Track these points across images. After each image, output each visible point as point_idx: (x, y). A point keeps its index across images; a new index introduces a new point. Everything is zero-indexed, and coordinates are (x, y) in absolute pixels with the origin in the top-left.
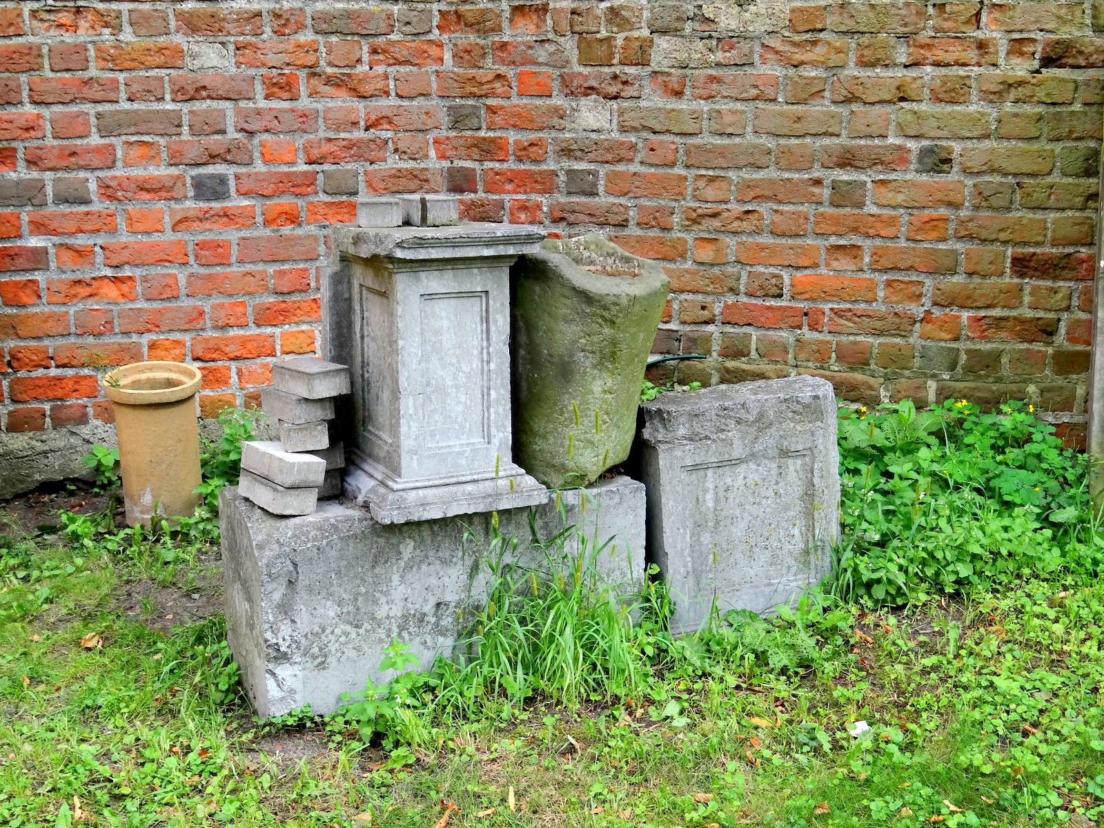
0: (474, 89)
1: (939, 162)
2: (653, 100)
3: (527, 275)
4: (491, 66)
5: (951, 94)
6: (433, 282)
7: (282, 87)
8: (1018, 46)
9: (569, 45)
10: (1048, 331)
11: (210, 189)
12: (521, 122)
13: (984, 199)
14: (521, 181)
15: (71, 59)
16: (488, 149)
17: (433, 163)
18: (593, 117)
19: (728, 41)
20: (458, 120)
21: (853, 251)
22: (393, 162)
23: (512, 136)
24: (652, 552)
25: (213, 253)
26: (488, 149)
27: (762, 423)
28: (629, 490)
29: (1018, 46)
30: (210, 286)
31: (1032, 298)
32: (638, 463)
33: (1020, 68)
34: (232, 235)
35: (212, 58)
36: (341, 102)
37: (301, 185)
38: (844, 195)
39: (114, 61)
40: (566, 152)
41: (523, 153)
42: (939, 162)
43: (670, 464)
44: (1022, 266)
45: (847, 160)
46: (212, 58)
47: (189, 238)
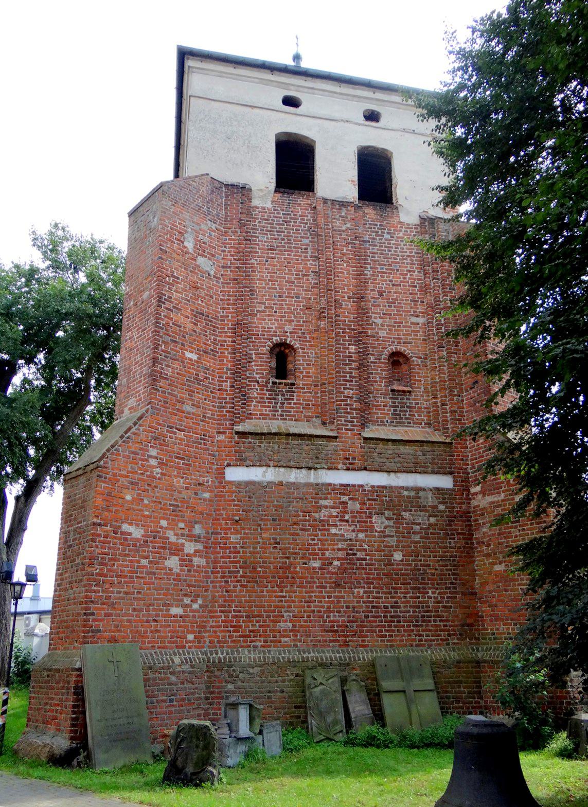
0: (210, 682)
1: (282, 691)
2: (240, 683)
3: (251, 706)
4: (213, 679)
5: (284, 681)
6: (243, 706)
7: (182, 683)
8: (292, 674)
9: (226, 675)
10: (299, 717)
11: (171, 701)
12: (218, 687)
13: (289, 697)
14: (218, 698)
15: (154, 679)
16: (212, 693)
17: (203, 695)
18: (230, 687)
19: (250, 674)
20: (207, 687)
21: (271, 706)
22: (197, 695)
23: (216, 690)
24: (263, 745)
25: (170, 712)
26: (212, 693)
27: (274, 727)
28: (261, 736)
29: (292, 674)
30: (169, 718)
31: (297, 712)
32: (261, 733)
33: (292, 677)
34: (173, 709)
35: (173, 679)
36: (190, 685)
37: (183, 700)
38: (269, 697)
39: (160, 679)
40: (226, 693)
41: (218, 693)
42: (282, 691)
43: (265, 732)
44: (295, 707)
45: (269, 692)
46: (173, 679)
47: (167, 710)
